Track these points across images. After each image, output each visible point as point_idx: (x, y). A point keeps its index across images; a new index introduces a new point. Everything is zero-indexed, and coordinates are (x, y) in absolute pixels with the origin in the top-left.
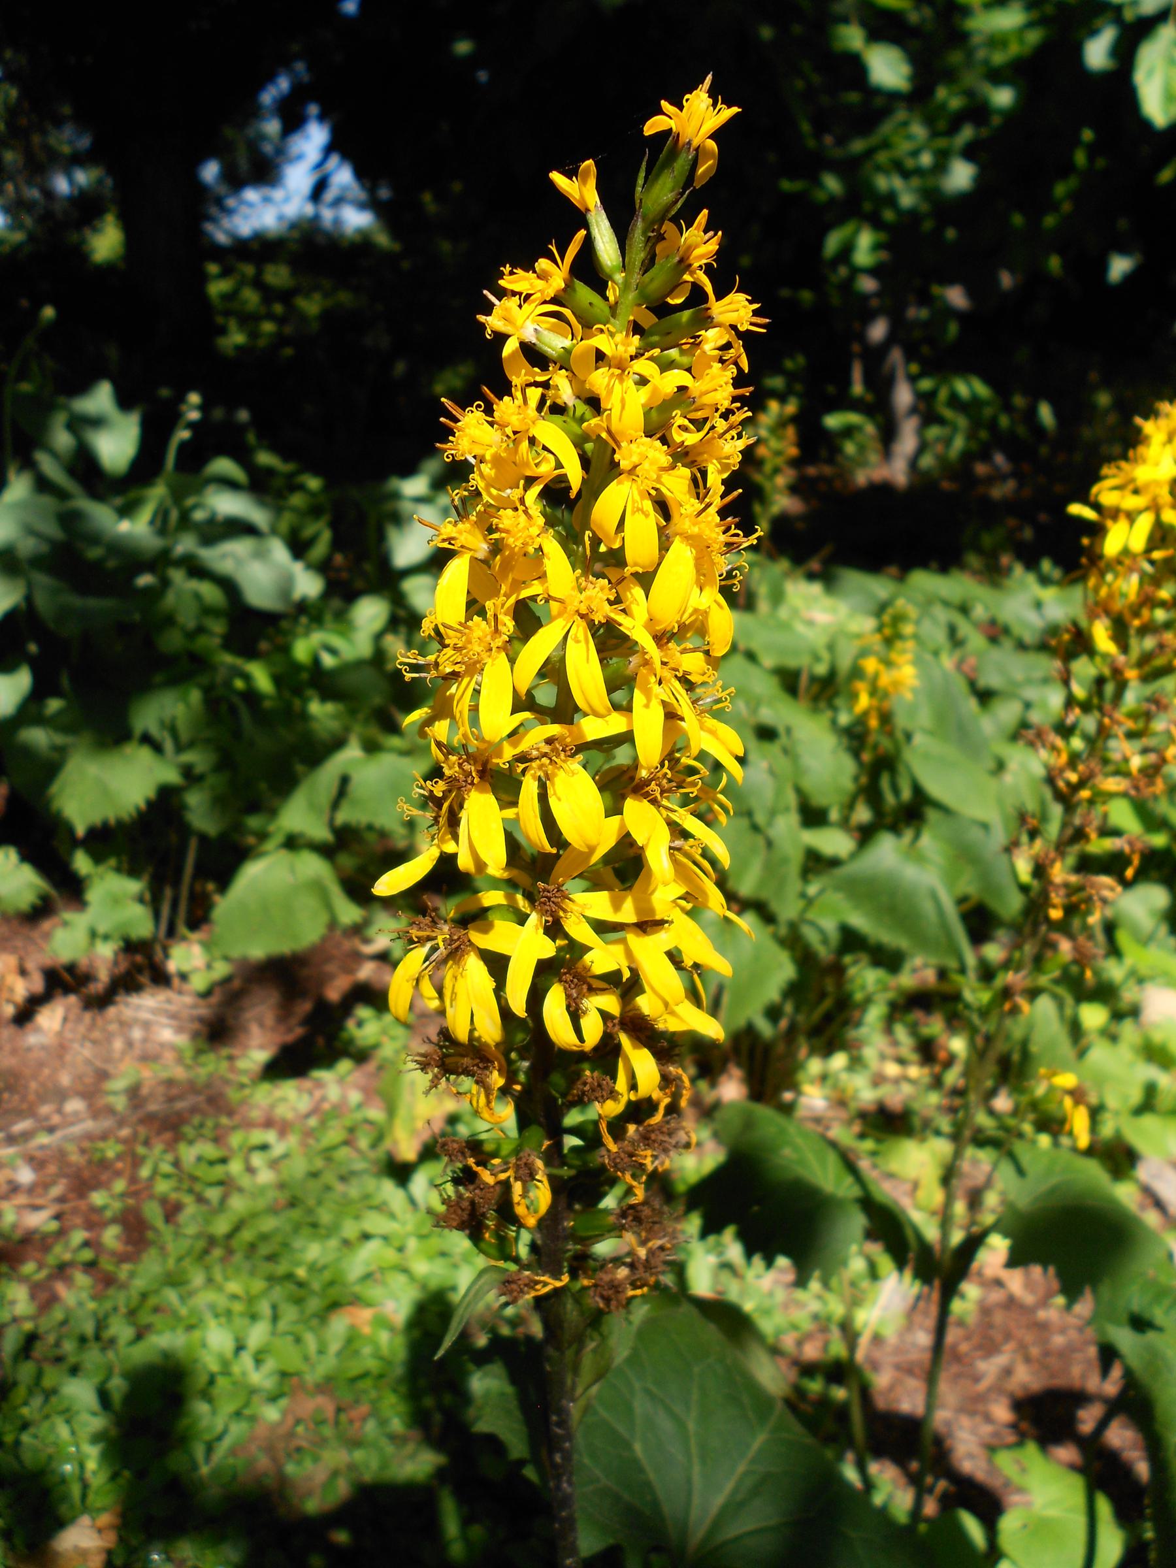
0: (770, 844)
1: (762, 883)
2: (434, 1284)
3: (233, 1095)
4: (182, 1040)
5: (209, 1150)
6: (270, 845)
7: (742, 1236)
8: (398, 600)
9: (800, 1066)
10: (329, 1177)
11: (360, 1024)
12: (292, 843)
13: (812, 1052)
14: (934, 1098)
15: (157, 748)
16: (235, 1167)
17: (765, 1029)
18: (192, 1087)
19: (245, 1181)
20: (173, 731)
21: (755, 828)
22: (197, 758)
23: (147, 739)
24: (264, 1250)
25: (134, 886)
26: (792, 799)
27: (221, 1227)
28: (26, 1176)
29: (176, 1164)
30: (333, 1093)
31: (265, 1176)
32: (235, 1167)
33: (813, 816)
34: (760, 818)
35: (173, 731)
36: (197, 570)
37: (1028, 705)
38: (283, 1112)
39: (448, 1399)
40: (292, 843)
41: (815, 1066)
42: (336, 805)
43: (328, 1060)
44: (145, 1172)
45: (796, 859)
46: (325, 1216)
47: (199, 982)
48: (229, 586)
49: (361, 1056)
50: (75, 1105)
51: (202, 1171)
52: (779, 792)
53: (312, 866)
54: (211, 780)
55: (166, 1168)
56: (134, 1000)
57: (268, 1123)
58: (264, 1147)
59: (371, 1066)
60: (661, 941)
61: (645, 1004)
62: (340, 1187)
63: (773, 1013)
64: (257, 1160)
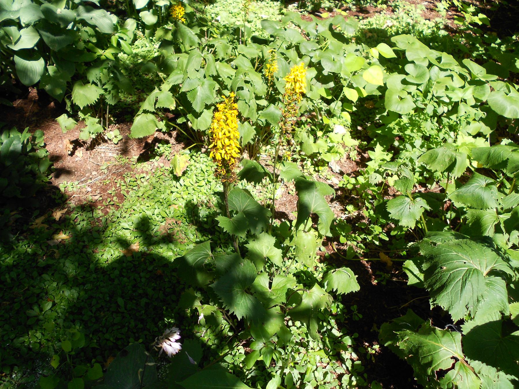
0: (249, 106)
1: (248, 114)
2: (188, 199)
3: (133, 167)
4: (115, 155)
5: (133, 179)
6: (139, 113)
7: (246, 180)
8: (138, 19)
9: (260, 148)
10: (161, 181)
11: (159, 148)
12: (145, 112)
13: (263, 145)
14: (289, 153)
15: (96, 85)
16: (139, 182)
17: (252, 143)
18: (121, 166)
19: (141, 185)
20: (100, 81)
21: (246, 103)
22: (108, 86)
23: (94, 83)
24: (151, 197)
25: (97, 120)
26: (254, 96)
27: (140, 194)
28: (89, 189)
29: (125, 182)
30: (156, 164)
31: (146, 183)
32: (139, 182)
33: (258, 98)
34: (247, 101)
35: (100, 81)
36: (84, 23)
37: (311, 58)
38: (144, 169)
39: (196, 218)
40: (145, 112)
41: (264, 148)
42: (155, 104)
43: (154, 156)
44: (118, 185)
45: (255, 107)
46: (162, 189)
47: (115, 141)
48: (94, 27)
49: (161, 155)
50: (94, 173)
51: (132, 183)
52: (251, 95)
53: (151, 117)
54: (112, 92)
55: (123, 184)
56: (100, 147)
57: (143, 172)
58: (144, 177)
59: (163, 157)
60: (234, 150)
61: (233, 155)
62: (164, 184)
63: (253, 140)
64: (142, 180)
